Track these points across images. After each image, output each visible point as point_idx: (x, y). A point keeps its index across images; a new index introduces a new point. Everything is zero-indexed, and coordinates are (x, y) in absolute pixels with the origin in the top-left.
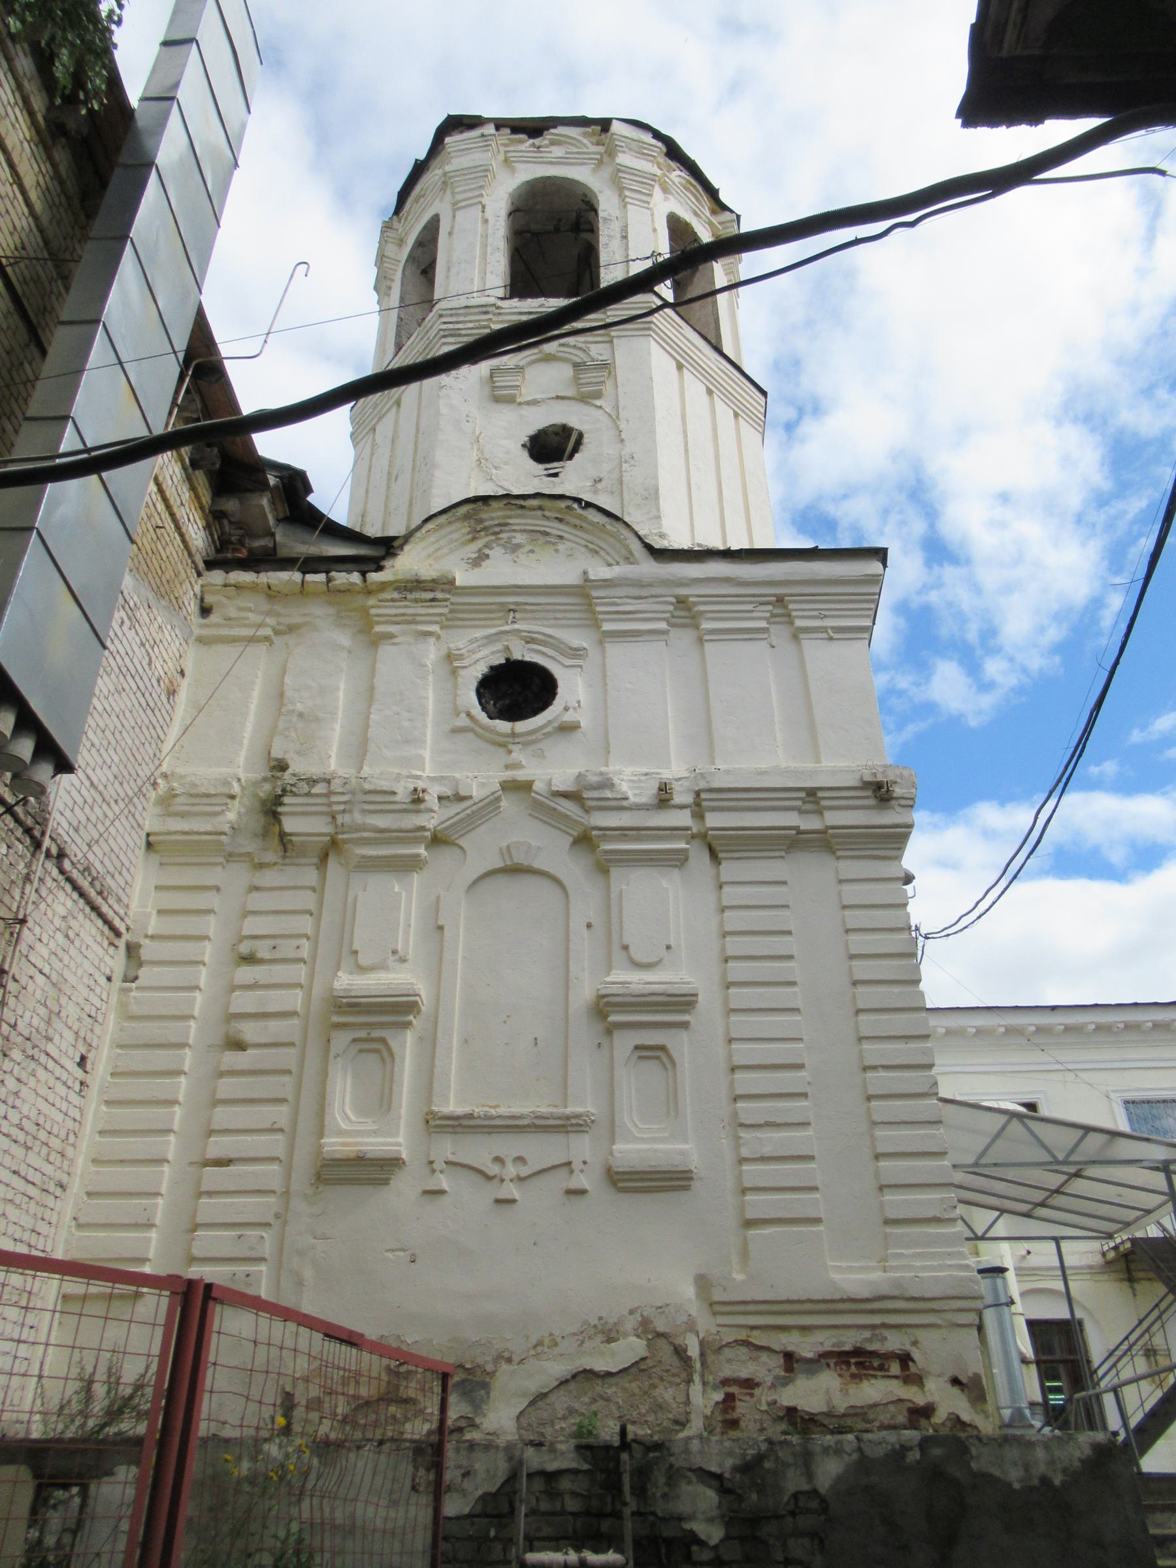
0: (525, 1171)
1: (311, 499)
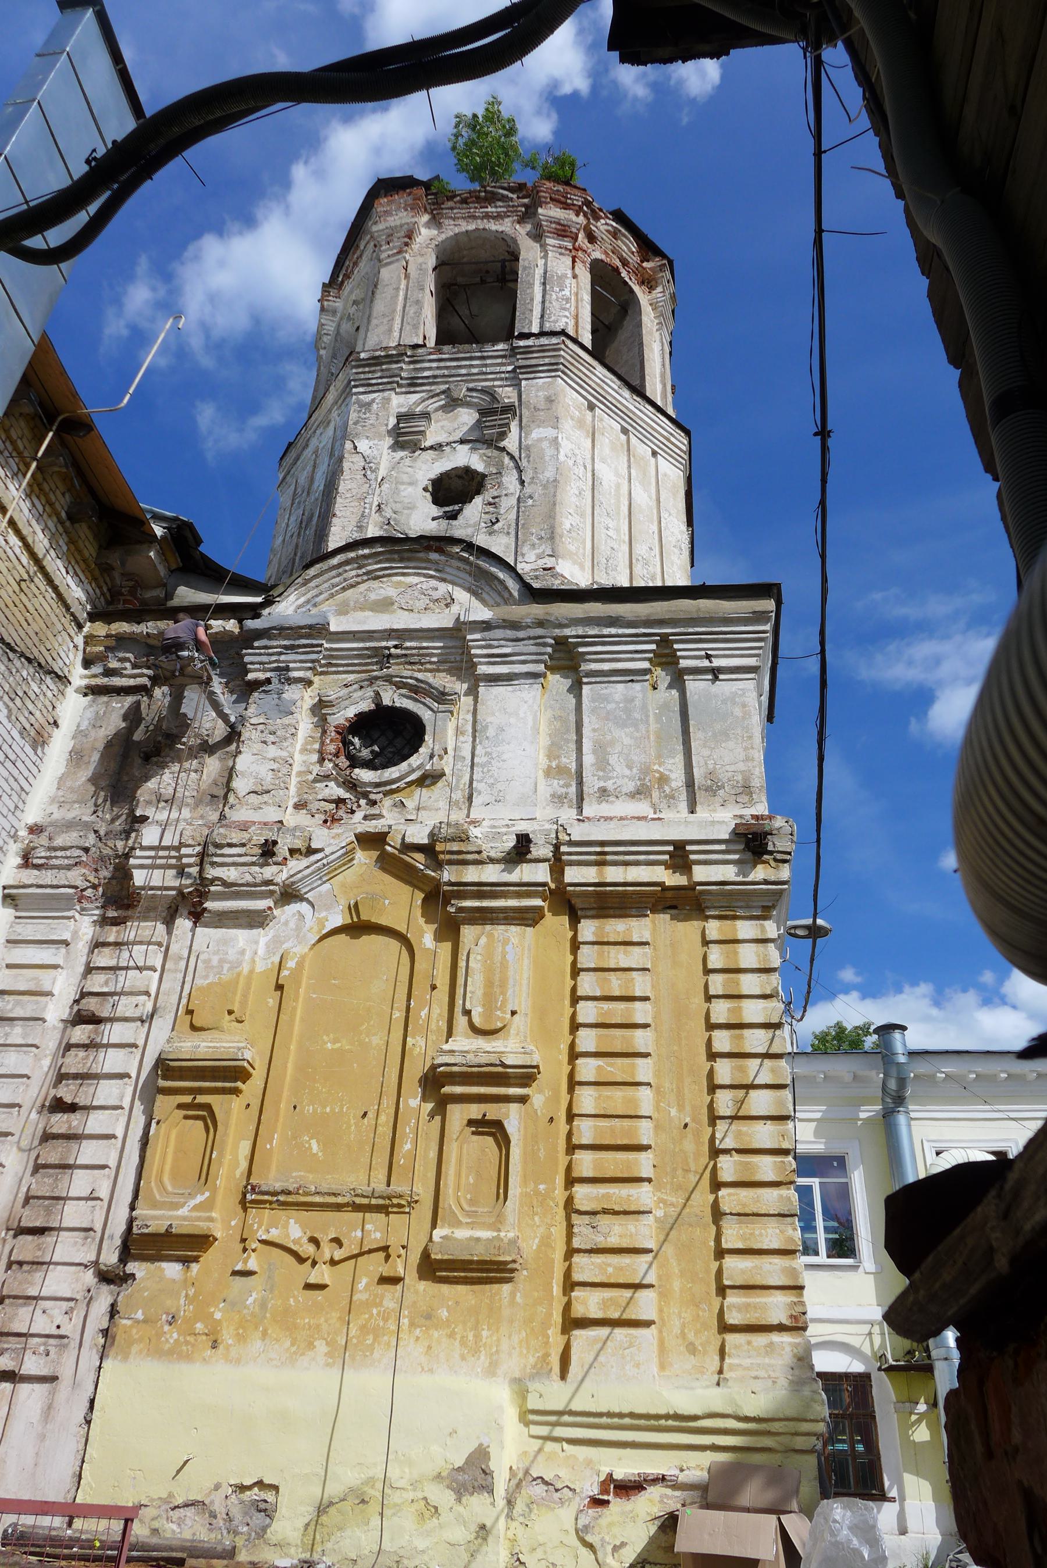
0: (338, 1255)
1: (202, 548)
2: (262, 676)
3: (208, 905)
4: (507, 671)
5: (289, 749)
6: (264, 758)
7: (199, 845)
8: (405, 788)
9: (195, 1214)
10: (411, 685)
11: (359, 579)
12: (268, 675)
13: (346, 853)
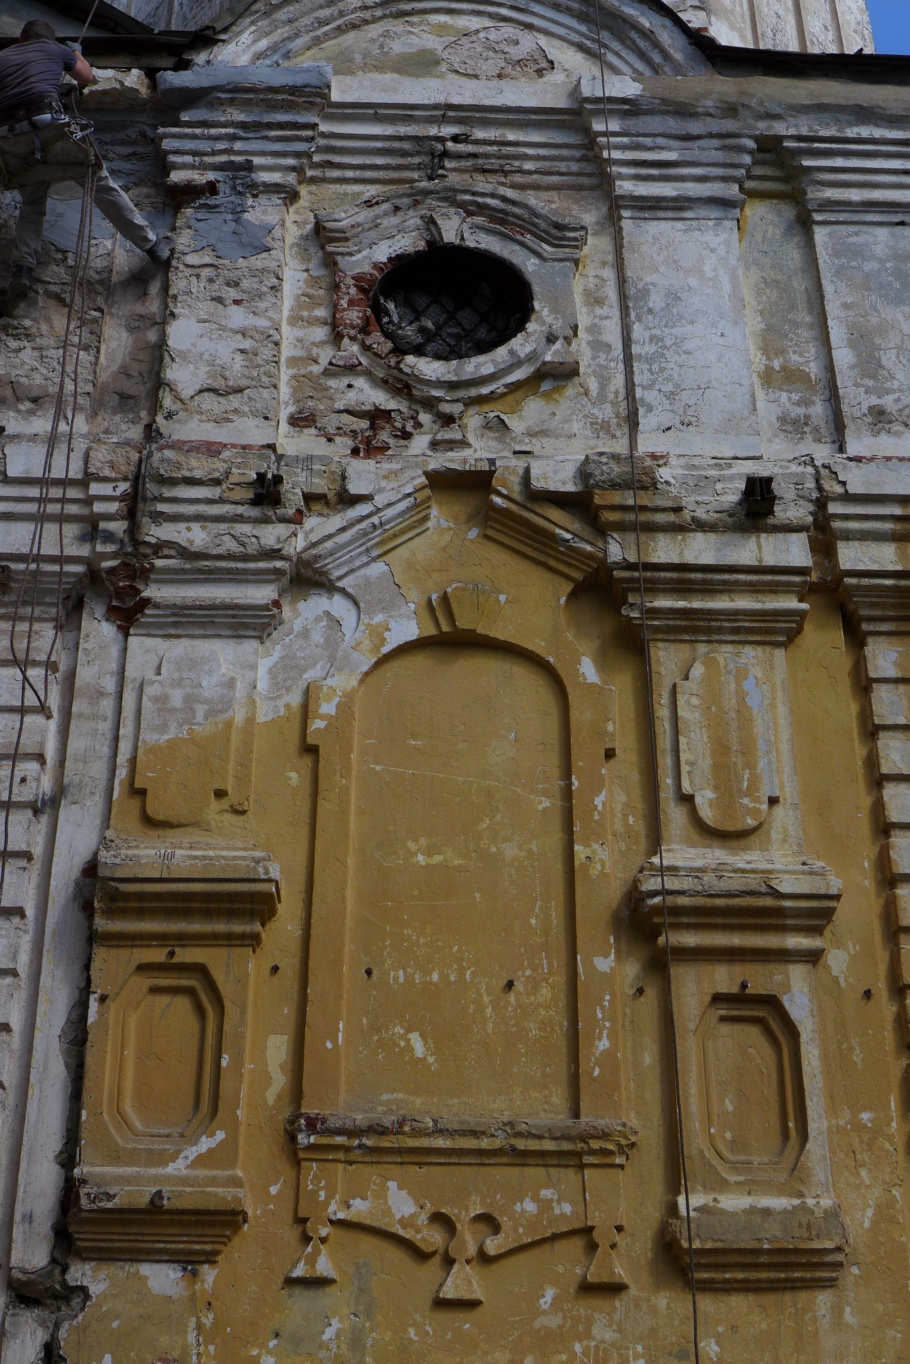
2: (200, 178)
3: (151, 592)
4: (674, 193)
5: (270, 314)
6: (224, 329)
7: (125, 479)
8: (503, 395)
9: (201, 1173)
10: (493, 209)
11: (367, 15)
12: (211, 176)
13: (416, 506)
